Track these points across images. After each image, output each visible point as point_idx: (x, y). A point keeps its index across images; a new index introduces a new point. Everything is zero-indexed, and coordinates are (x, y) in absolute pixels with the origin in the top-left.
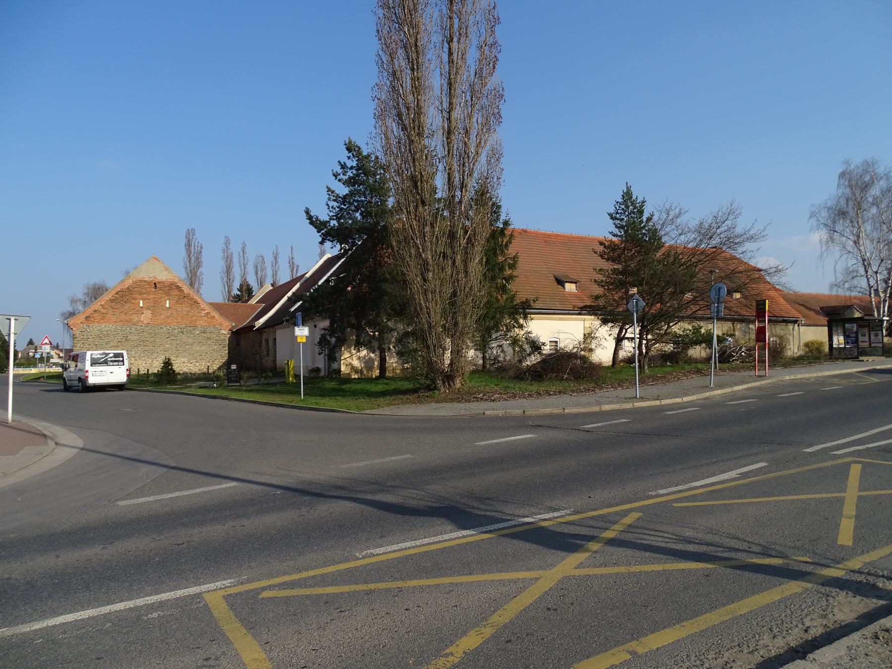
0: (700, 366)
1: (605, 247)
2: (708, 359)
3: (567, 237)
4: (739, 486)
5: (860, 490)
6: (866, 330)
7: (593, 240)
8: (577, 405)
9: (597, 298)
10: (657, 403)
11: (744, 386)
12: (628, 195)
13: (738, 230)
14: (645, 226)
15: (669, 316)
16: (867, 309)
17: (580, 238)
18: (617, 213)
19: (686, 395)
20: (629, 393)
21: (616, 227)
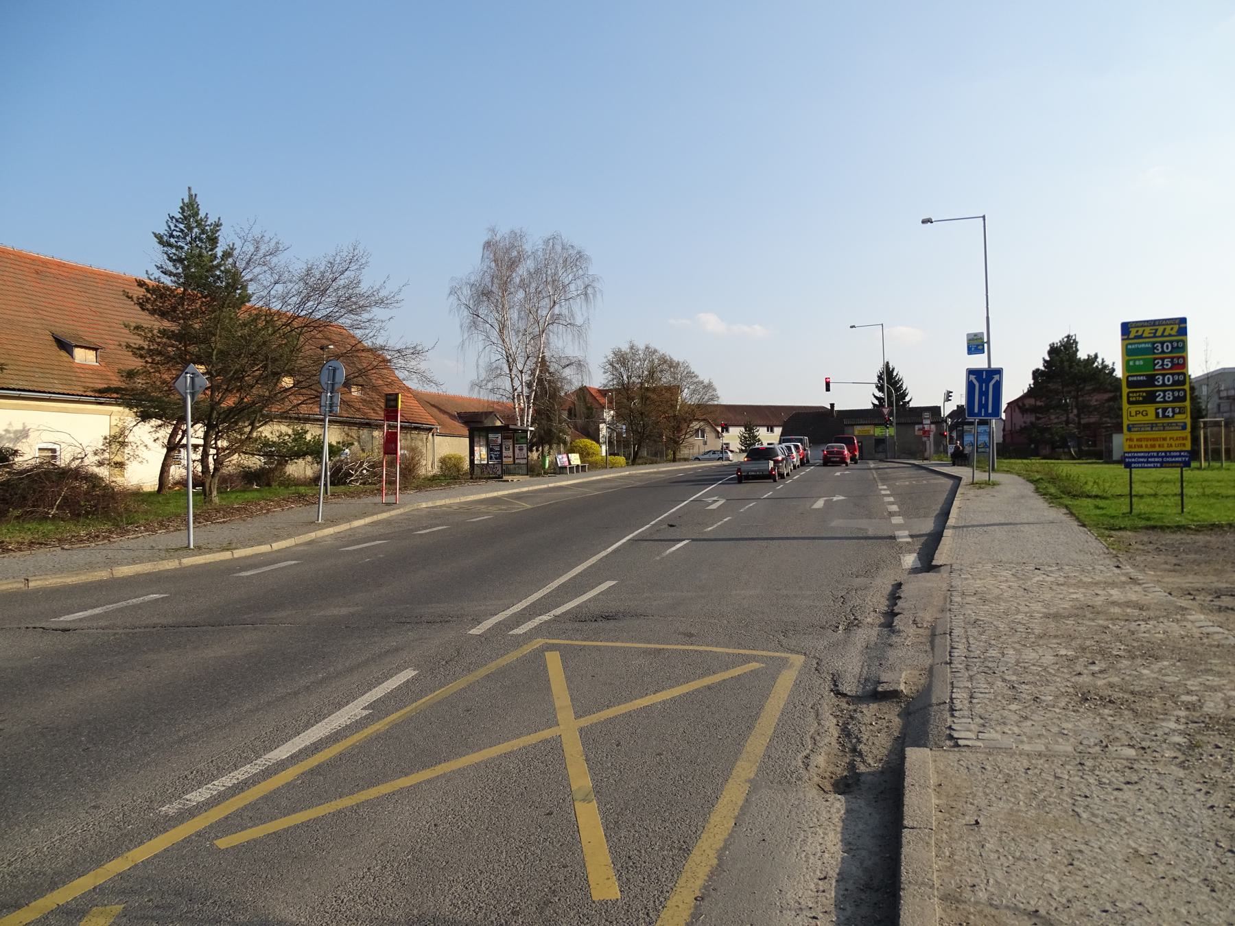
0: (302, 489)
1: (148, 290)
2: (316, 480)
3: (81, 270)
4: (370, 741)
5: (578, 716)
6: (510, 443)
7: (125, 280)
8: (56, 571)
9: (131, 374)
10: (226, 555)
11: (368, 520)
12: (190, 209)
13: (364, 287)
14: (219, 265)
15: (254, 413)
16: (510, 417)
17: (107, 275)
18: (171, 236)
19: (277, 538)
20: (175, 539)
21: (170, 259)
